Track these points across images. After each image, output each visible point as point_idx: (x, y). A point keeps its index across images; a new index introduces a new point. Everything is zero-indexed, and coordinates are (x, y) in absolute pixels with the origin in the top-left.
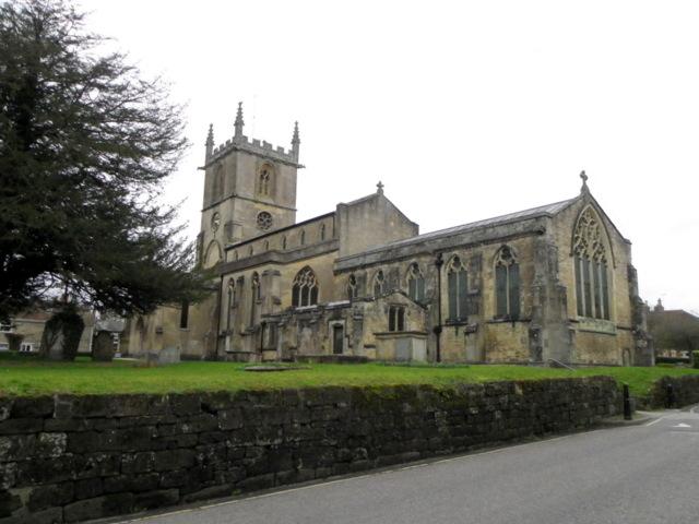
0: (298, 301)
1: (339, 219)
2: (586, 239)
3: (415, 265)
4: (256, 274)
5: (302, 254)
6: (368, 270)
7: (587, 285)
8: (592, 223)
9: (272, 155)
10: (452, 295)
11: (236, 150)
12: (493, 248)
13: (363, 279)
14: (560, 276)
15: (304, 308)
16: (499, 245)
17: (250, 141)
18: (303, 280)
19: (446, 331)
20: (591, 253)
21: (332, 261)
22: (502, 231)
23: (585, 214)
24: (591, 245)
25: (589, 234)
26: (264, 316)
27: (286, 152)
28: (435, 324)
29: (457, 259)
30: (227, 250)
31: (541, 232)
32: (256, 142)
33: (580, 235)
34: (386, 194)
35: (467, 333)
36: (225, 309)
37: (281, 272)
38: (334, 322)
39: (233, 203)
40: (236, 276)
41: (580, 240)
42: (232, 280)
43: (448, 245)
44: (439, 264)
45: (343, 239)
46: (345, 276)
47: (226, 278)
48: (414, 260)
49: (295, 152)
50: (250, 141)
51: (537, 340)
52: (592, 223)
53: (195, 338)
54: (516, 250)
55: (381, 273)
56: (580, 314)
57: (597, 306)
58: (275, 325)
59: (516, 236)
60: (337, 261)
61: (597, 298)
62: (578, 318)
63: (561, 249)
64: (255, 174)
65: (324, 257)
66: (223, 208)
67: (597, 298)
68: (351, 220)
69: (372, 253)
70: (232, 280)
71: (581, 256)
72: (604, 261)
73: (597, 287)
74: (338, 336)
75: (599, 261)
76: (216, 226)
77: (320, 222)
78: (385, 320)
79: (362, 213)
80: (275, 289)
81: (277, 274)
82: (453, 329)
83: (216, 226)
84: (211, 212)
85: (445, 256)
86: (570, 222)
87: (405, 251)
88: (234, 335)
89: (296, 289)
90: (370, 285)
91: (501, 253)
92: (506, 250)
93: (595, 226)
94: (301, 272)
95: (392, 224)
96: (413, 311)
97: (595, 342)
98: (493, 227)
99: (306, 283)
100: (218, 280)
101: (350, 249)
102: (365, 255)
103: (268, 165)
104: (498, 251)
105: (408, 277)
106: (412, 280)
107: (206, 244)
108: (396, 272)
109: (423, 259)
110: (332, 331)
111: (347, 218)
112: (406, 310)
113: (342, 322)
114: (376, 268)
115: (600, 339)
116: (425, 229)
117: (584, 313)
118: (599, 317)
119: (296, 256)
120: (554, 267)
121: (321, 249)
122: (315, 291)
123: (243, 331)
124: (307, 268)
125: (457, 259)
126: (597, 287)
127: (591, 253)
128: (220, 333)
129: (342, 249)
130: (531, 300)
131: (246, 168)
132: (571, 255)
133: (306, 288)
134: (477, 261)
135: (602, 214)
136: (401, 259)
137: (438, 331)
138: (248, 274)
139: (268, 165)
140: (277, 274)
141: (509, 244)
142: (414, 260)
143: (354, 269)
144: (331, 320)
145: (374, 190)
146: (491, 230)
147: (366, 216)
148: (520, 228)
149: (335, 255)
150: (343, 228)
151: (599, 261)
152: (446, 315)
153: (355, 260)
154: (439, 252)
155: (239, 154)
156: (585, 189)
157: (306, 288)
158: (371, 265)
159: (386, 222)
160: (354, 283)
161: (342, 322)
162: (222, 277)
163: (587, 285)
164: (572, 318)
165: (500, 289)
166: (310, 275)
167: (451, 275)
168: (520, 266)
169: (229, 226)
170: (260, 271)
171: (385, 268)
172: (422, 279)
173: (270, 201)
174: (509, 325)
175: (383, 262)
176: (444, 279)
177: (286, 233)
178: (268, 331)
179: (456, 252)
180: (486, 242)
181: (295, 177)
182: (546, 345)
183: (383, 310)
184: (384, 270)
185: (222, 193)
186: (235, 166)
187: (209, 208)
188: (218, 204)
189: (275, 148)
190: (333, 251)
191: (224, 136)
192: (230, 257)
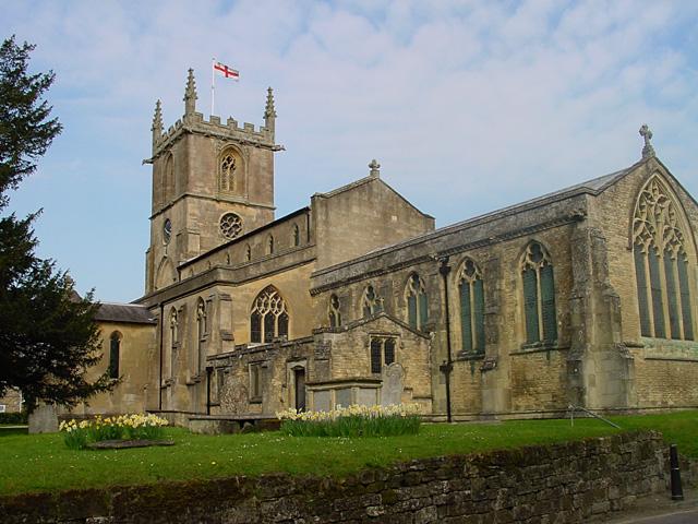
0: (259, 335)
1: (315, 218)
2: (653, 224)
3: (415, 276)
4: (201, 300)
5: (263, 269)
6: (353, 286)
7: (656, 291)
8: (661, 200)
9: (237, 135)
10: (466, 315)
11: (186, 132)
12: (516, 245)
13: (347, 299)
14: (611, 280)
15: (256, 345)
16: (525, 240)
17: (206, 119)
18: (266, 305)
19: (459, 369)
20: (661, 244)
21: (307, 276)
22: (528, 219)
23: (49, 132)
24: (660, 234)
25: (657, 216)
26: (211, 359)
27: (257, 130)
28: (441, 359)
29: (469, 263)
30: (180, 269)
31: (579, 219)
32: (216, 120)
33: (644, 219)
34: (384, 175)
35: (483, 371)
36: (169, 351)
37: (232, 296)
38: (294, 364)
39: (185, 204)
40: (178, 304)
41: (642, 225)
42: (174, 309)
43: (455, 243)
44: (445, 271)
45: (321, 245)
46: (324, 296)
47: (167, 308)
48: (412, 268)
49: (269, 128)
50: (224, 122)
51: (579, 377)
52: (661, 200)
53: (130, 391)
54: (548, 246)
55: (370, 288)
56: (646, 334)
57: (673, 320)
58: (223, 371)
59: (546, 225)
60: (314, 276)
61: (672, 310)
62: (642, 340)
63: (612, 241)
64: (216, 163)
65: (295, 271)
66: (174, 213)
67: (672, 310)
68: (332, 215)
69: (356, 262)
70: (174, 309)
71: (645, 249)
72: (682, 255)
73: (671, 292)
74: (300, 384)
75: (674, 256)
76: (167, 237)
77: (291, 222)
78: (366, 358)
79: (349, 207)
80: (223, 319)
81: (227, 298)
82: (467, 365)
83: (167, 237)
84: (161, 218)
85: (452, 261)
86: (624, 201)
87: (400, 257)
88: (178, 385)
89: (255, 319)
90: (357, 308)
91: (528, 250)
92: (535, 246)
93: (667, 203)
94: (261, 295)
95: (394, 218)
96: (407, 343)
97: (669, 375)
98: (515, 214)
99: (270, 308)
100: (157, 311)
101: (334, 258)
102: (348, 265)
103: (231, 149)
104: (524, 249)
105: (406, 294)
106: (412, 298)
107: (157, 263)
108: (386, 289)
109: (424, 266)
110: (292, 377)
111: (327, 215)
112: (398, 340)
113: (303, 364)
114: (364, 283)
115: (679, 367)
116: (439, 225)
117: (682, 335)
118: (675, 336)
119: (253, 272)
120: (600, 267)
121: (289, 261)
122: (283, 321)
123: (188, 380)
124: (269, 289)
125: (469, 263)
126: (671, 292)
127: (661, 244)
128: (163, 384)
129: (321, 257)
130: (568, 318)
131: (201, 155)
132: (629, 249)
133: (270, 317)
134: (494, 267)
135: (677, 187)
136: (394, 268)
137: (447, 369)
138: (191, 300)
139: (231, 149)
140: (227, 298)
141: (537, 238)
142: (412, 268)
143: (335, 285)
144: (288, 361)
145: (366, 173)
146: (513, 218)
147: (355, 210)
148: (552, 214)
149: (311, 268)
150: (320, 228)
151: (674, 256)
152: (457, 346)
153: (337, 273)
154: (445, 254)
155: (192, 137)
156: (647, 150)
157: (270, 317)
158: (357, 279)
159: (386, 216)
160: (336, 306)
161: (303, 364)
162: (162, 306)
163: (656, 291)
164: (627, 340)
165: (530, 303)
166: (276, 297)
167: (463, 286)
168: (555, 269)
169: (182, 238)
170: (205, 295)
171: (375, 281)
172: (425, 295)
173: (240, 199)
174: (543, 356)
175: (370, 274)
176: (454, 292)
177: (250, 241)
178: (215, 379)
179: (467, 254)
180: (507, 236)
181: (271, 164)
182: (593, 384)
183: (361, 343)
184: (373, 285)
185: (173, 192)
186: (187, 154)
187: (158, 214)
188: (169, 207)
189: (241, 126)
190: (306, 262)
191: (173, 116)
192: (185, 274)
